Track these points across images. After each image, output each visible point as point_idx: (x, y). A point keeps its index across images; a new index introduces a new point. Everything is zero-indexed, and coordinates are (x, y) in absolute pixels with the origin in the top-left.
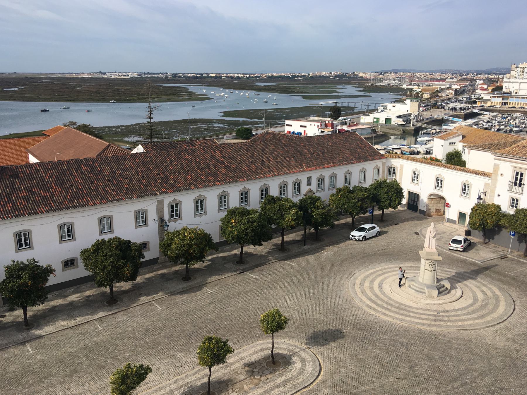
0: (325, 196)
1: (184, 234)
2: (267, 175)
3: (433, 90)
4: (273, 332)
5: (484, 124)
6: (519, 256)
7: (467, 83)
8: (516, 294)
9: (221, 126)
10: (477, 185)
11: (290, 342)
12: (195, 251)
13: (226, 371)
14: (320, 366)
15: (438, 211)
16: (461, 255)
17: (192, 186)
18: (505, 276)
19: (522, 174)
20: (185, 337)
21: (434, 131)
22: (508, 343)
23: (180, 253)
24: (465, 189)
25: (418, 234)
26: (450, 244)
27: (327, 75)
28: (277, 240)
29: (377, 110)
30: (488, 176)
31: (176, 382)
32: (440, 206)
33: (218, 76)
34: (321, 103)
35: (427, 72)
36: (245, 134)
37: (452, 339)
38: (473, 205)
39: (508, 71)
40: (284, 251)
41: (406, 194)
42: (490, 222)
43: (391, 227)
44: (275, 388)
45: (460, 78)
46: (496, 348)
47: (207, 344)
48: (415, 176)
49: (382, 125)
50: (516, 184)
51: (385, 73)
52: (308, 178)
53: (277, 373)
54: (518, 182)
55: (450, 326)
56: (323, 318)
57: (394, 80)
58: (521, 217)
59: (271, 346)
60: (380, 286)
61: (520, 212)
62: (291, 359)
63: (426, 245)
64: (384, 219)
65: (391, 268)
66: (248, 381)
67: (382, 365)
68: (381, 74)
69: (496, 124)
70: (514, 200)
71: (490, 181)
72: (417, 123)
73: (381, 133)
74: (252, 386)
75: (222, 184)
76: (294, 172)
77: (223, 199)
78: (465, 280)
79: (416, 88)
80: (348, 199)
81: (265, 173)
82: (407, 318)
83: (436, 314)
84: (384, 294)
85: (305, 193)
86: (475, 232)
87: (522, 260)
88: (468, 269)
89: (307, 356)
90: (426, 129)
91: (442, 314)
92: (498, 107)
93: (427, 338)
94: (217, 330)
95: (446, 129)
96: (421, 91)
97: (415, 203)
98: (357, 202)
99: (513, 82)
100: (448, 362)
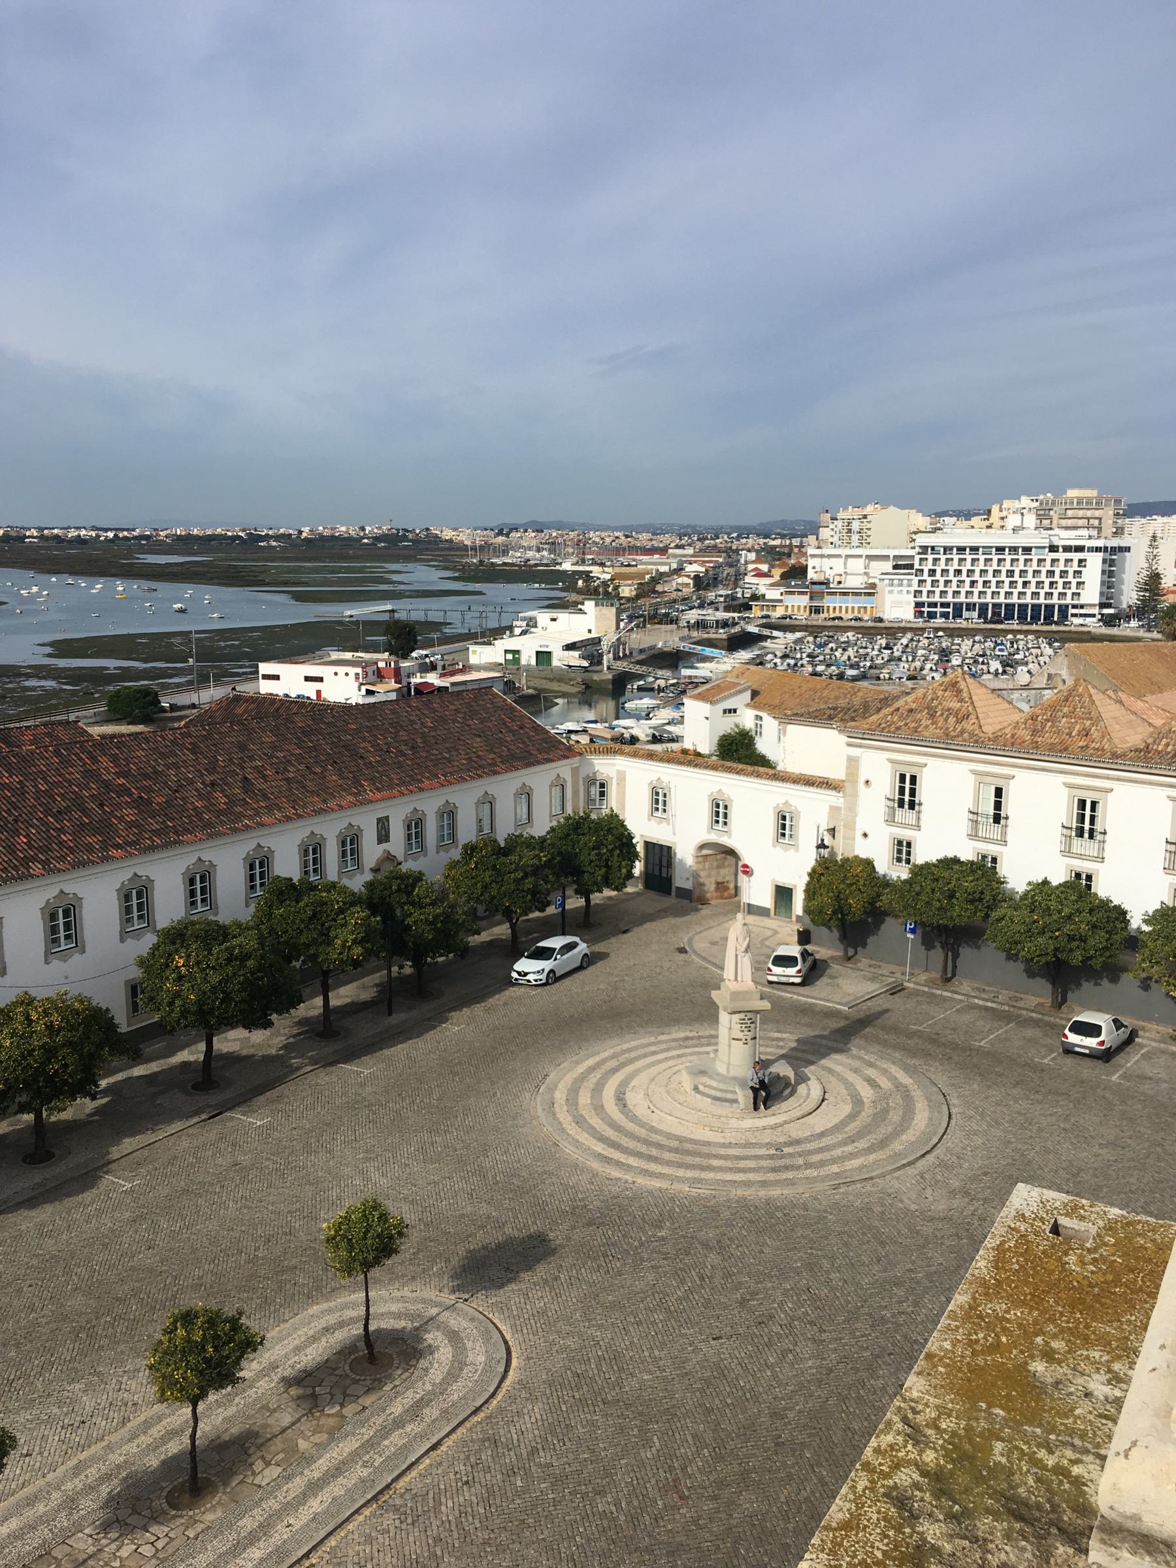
0: (432, 865)
1: (28, 1017)
2: (265, 819)
3: (641, 575)
4: (367, 1266)
5: (778, 661)
6: (930, 983)
7: (721, 560)
8: (945, 1078)
9: (50, 684)
10: (814, 811)
11: (406, 1292)
12: (66, 1066)
13: (232, 1410)
14: (506, 1342)
15: (721, 886)
16: (799, 994)
17: (36, 868)
18: (911, 1035)
19: (913, 779)
20: (76, 1333)
21: (662, 683)
22: (956, 1203)
23: (16, 1079)
24: (784, 825)
25: (686, 952)
26: (770, 970)
27: (353, 533)
28: (312, 1007)
29: (511, 628)
30: (835, 788)
31: (77, 1470)
32: (726, 874)
33: (13, 534)
34: (348, 613)
35: (614, 529)
36: (140, 705)
37: (825, 1211)
38: (812, 863)
39: (813, 528)
40: (335, 1038)
41: (640, 848)
42: (854, 902)
43: (613, 940)
44: (392, 1430)
45: (699, 545)
46: (932, 1219)
47: (181, 1332)
48: (659, 800)
49: (528, 668)
50: (901, 804)
51: (511, 530)
52: (379, 820)
53: (387, 1388)
54: (907, 798)
55: (814, 1180)
56: (484, 1209)
57: (539, 550)
58: (928, 885)
59: (362, 1311)
60: (620, 1099)
61: (921, 871)
62: (420, 1340)
63: (729, 973)
64: (592, 920)
65: (636, 1048)
66: (306, 1425)
67: (668, 1310)
68: (500, 533)
69: (804, 662)
70: (900, 843)
71: (842, 800)
72: (619, 663)
73: (530, 691)
74: (321, 1438)
75: (131, 854)
76: (341, 807)
77: (136, 901)
78: (824, 1056)
79: (596, 571)
80: (498, 873)
81: (258, 814)
82: (705, 1175)
83: (772, 1152)
84: (634, 1119)
85: (373, 865)
86: (820, 932)
87: (939, 992)
88: (824, 1029)
89: (464, 1324)
90: (641, 677)
91: (787, 1150)
92: (802, 617)
93: (766, 1219)
94: (174, 1297)
95: (690, 677)
96: (612, 580)
97: (664, 870)
98: (523, 878)
99: (829, 556)
100: (828, 1272)
